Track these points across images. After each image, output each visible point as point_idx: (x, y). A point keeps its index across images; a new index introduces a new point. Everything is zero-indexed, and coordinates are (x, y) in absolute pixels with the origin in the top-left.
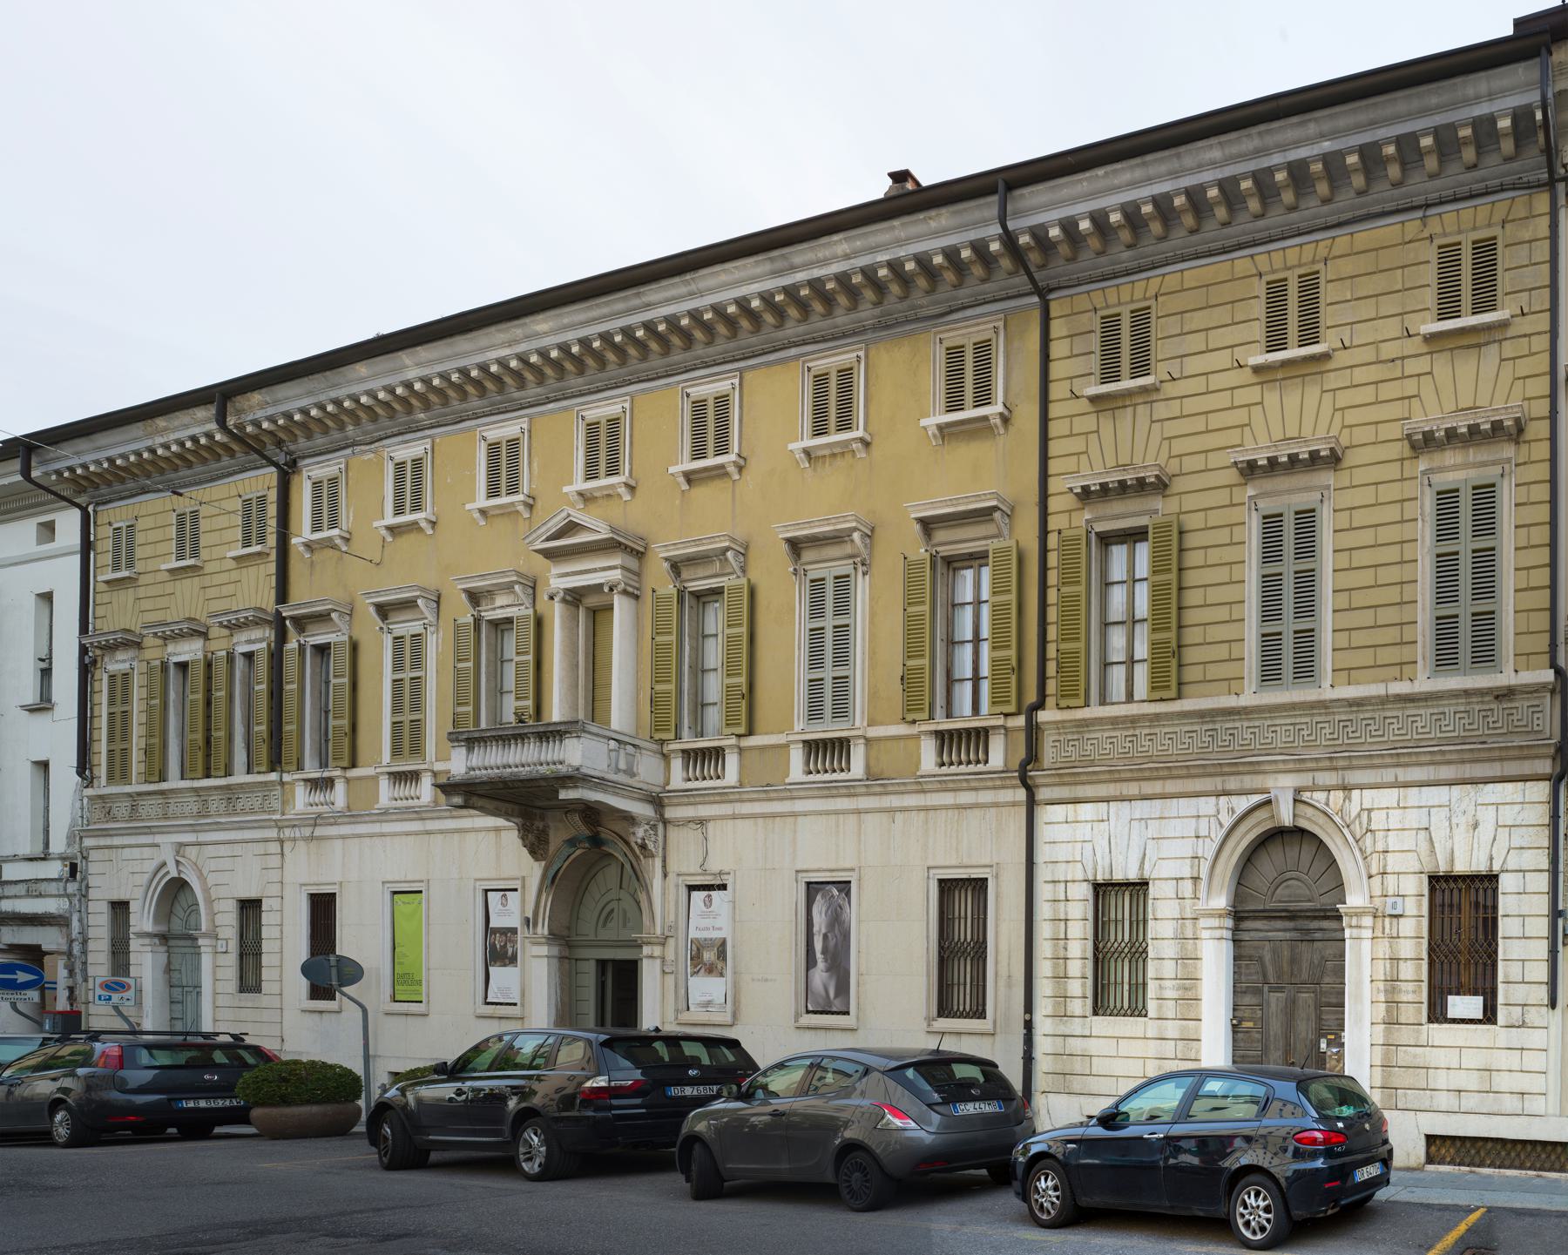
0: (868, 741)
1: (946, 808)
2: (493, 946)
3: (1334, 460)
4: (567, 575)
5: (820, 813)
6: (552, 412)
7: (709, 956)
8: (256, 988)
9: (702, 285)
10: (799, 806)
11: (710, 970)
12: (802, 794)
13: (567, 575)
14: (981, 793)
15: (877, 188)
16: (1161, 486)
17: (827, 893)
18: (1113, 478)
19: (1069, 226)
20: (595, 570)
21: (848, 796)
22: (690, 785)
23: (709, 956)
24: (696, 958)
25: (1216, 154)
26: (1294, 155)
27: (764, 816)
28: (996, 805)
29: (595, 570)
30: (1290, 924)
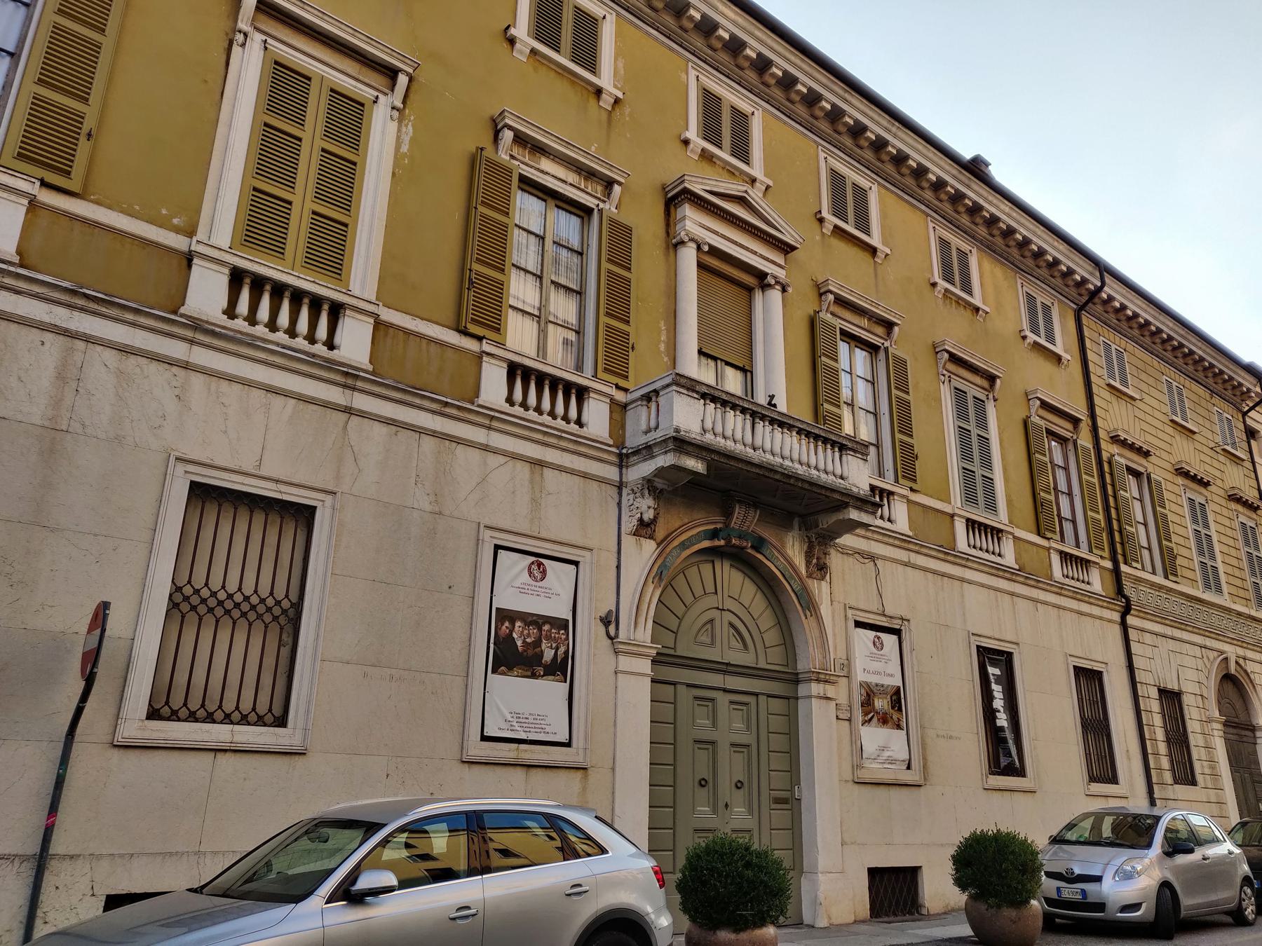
0: (379, 325)
1: (1071, 610)
2: (509, 639)
3: (1206, 485)
4: (708, 229)
5: (983, 585)
6: (650, 35)
7: (881, 704)
8: (1018, 771)
9: (900, 134)
10: (969, 574)
11: (884, 720)
12: (975, 566)
13: (708, 229)
14: (197, 349)
15: (967, 154)
16: (1146, 454)
17: (995, 663)
18: (1138, 443)
19: (1123, 307)
20: (755, 253)
21: (345, 386)
22: (973, 552)
23: (881, 704)
24: (867, 703)
25: (1171, 325)
26: (1194, 348)
27: (935, 572)
28: (1101, 618)
29: (755, 253)
30: (1235, 731)
